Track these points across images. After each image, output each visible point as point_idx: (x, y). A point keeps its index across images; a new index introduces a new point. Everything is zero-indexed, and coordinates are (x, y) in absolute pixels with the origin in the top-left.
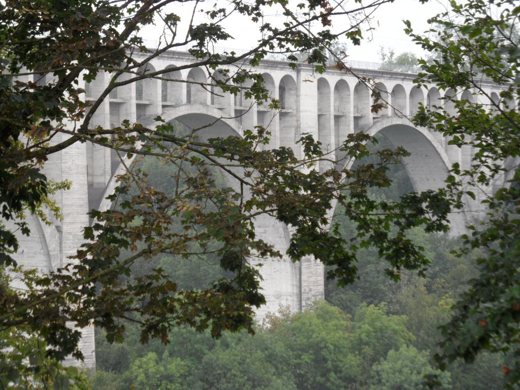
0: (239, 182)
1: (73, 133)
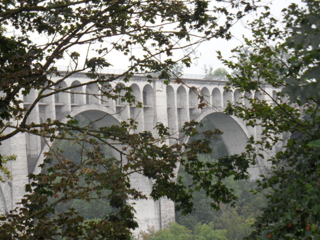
0: (120, 153)
1: (16, 127)
